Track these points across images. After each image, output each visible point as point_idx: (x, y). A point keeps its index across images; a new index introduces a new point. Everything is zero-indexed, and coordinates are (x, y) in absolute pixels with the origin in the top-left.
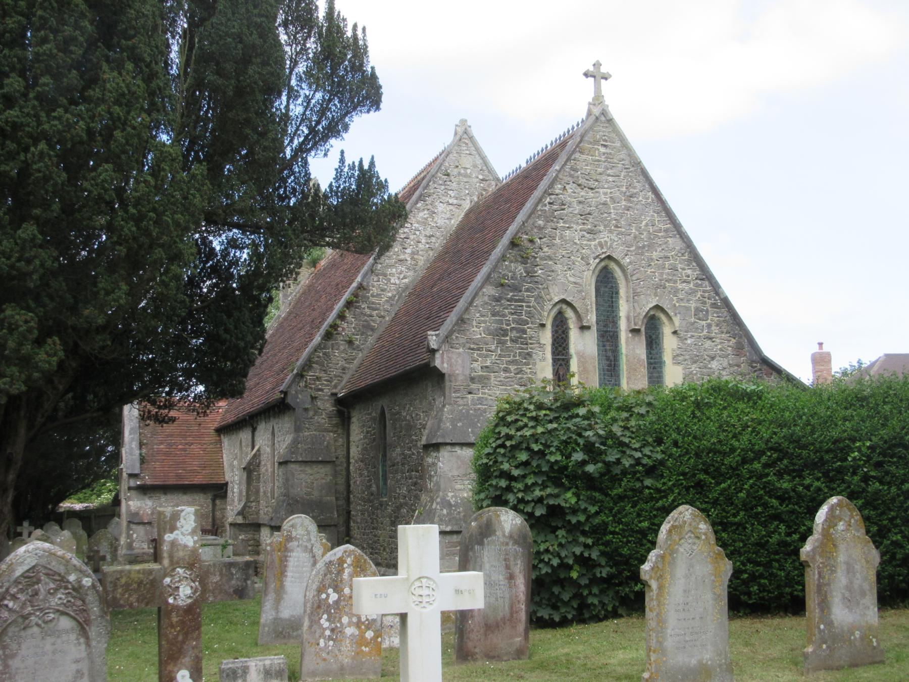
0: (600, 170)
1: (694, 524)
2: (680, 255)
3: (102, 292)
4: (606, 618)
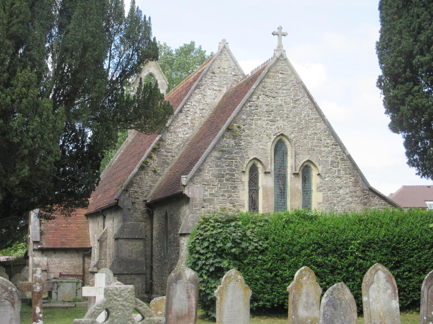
0: (278, 87)
1: (235, 276)
2: (323, 132)
3: (18, 170)
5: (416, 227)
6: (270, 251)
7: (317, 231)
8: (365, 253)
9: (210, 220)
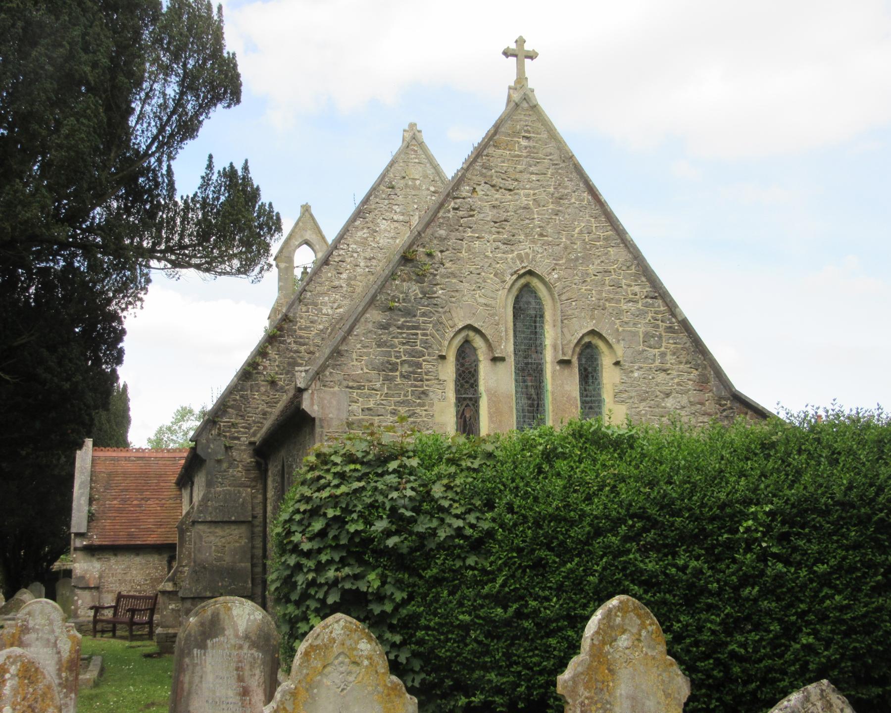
0: (519, 167)
1: (348, 643)
2: (624, 268)
6: (499, 542)
8: (789, 541)
9: (333, 458)
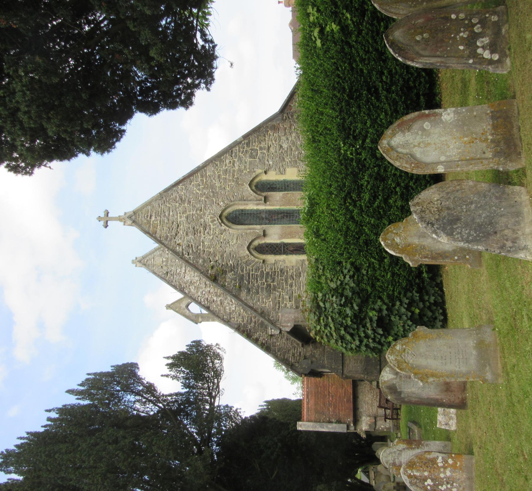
1: (397, 353)
2: (217, 167)
4: (442, 291)
5: (321, 65)
7: (328, 199)
